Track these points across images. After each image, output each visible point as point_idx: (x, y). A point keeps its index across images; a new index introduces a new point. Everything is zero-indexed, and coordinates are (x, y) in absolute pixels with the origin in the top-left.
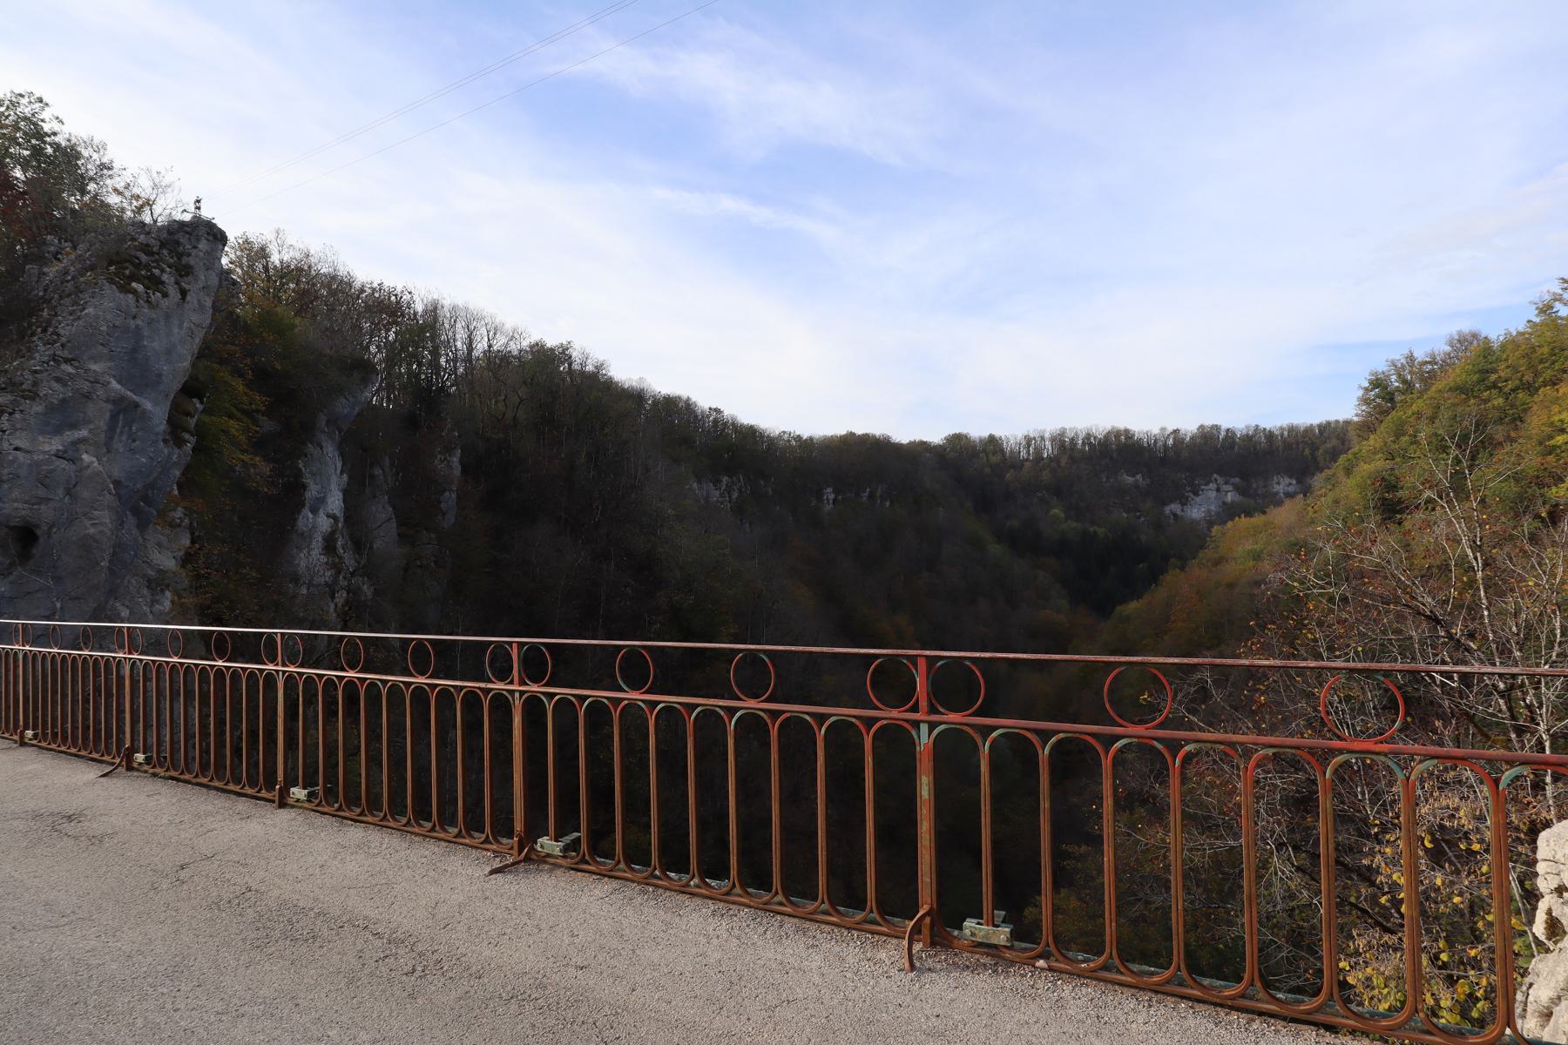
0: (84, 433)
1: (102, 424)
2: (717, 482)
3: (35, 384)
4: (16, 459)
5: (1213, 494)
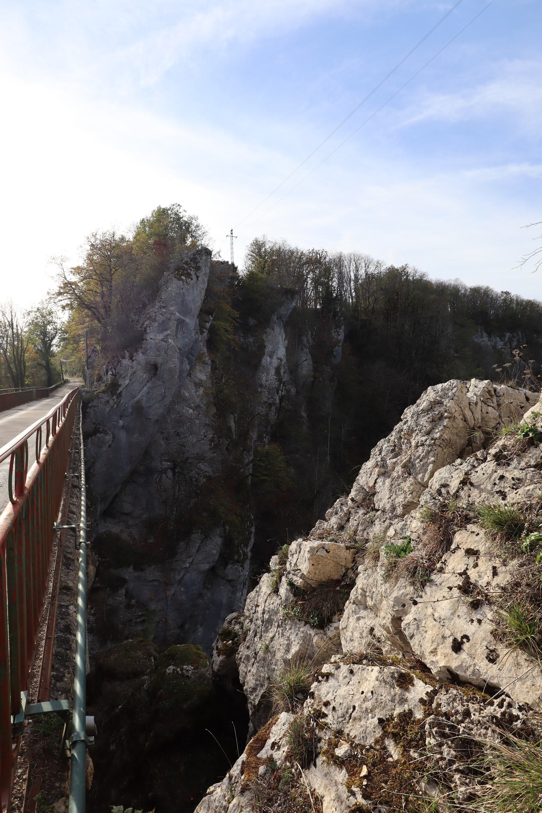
0: (169, 332)
1: (174, 328)
2: (502, 337)
3: (156, 316)
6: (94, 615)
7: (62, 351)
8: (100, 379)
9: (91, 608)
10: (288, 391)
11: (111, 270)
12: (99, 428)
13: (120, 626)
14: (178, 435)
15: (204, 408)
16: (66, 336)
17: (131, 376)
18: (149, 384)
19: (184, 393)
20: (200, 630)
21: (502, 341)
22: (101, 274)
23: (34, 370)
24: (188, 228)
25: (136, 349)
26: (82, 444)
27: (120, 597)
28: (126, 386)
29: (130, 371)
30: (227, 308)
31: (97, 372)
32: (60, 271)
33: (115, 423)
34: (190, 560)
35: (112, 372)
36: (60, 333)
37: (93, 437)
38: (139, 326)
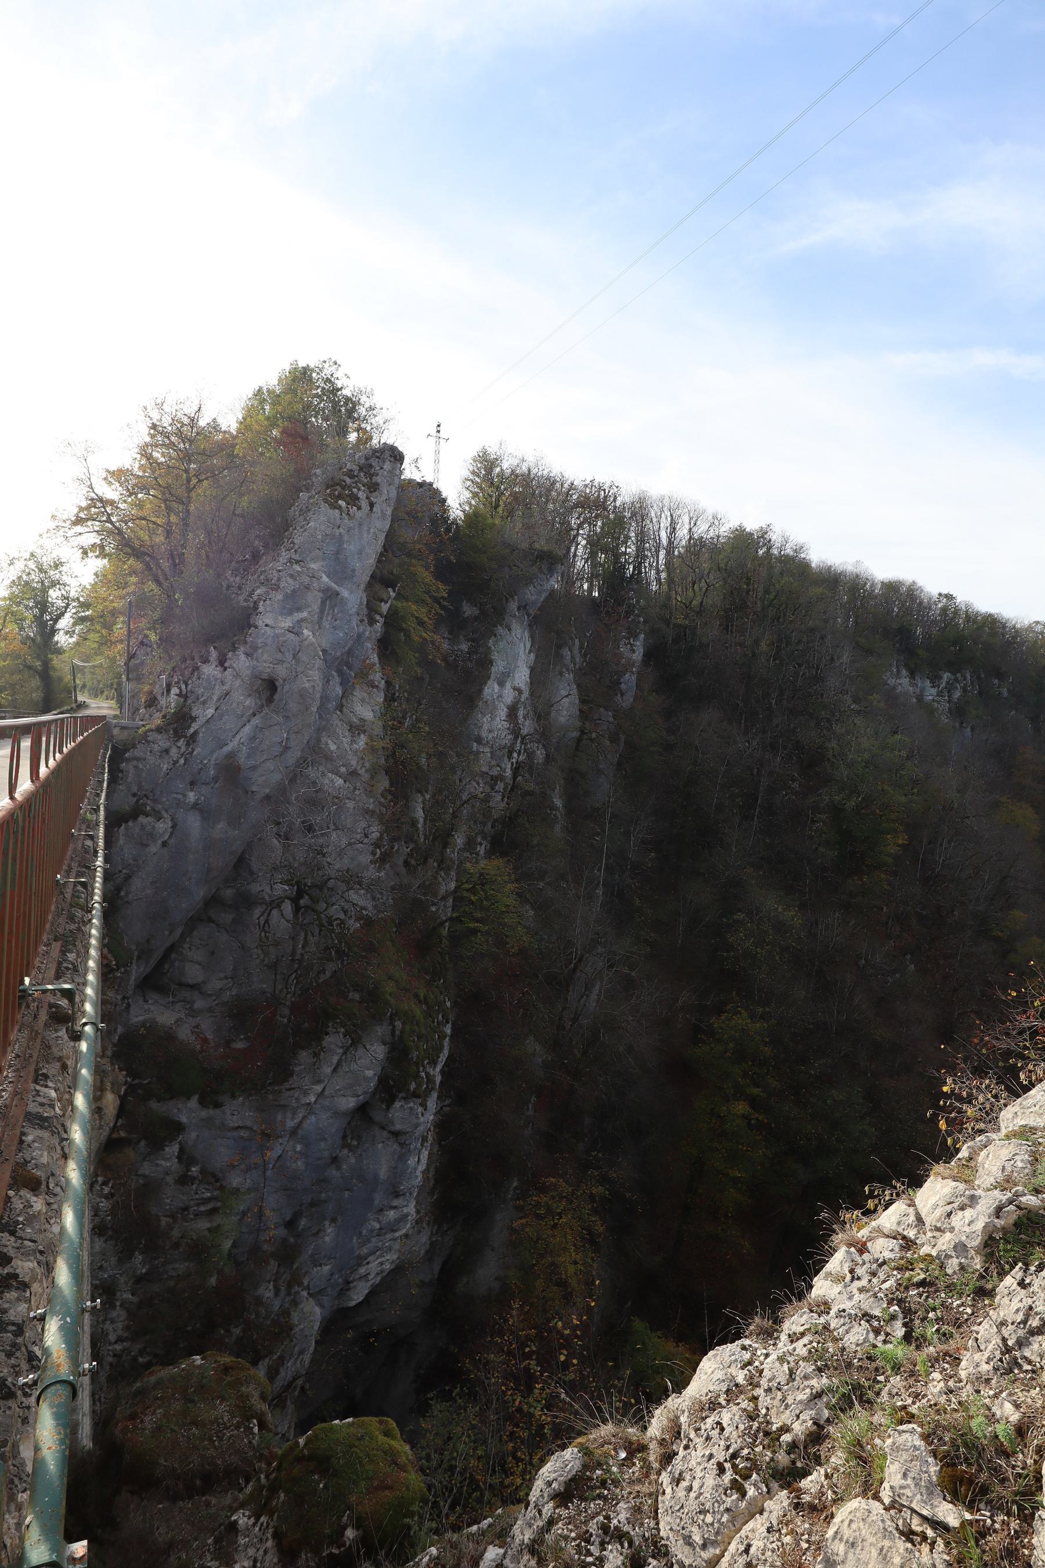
0: (305, 614)
1: (316, 607)
2: (935, 679)
3: (279, 580)
6: (109, 1196)
7: (77, 644)
8: (152, 702)
9: (105, 1183)
10: (530, 755)
11: (189, 480)
12: (145, 805)
13: (164, 1221)
14: (310, 829)
15: (366, 777)
16: (87, 613)
17: (219, 700)
18: (256, 721)
19: (327, 744)
20: (329, 1231)
21: (934, 687)
22: (168, 487)
23: (16, 677)
24: (350, 412)
25: (233, 644)
26: (101, 853)
27: (166, 1160)
28: (207, 721)
29: (218, 691)
30: (426, 576)
31: (147, 688)
32: (81, 472)
33: (180, 796)
34: (318, 1088)
35: (180, 688)
36: (74, 607)
37: (130, 824)
38: (241, 598)
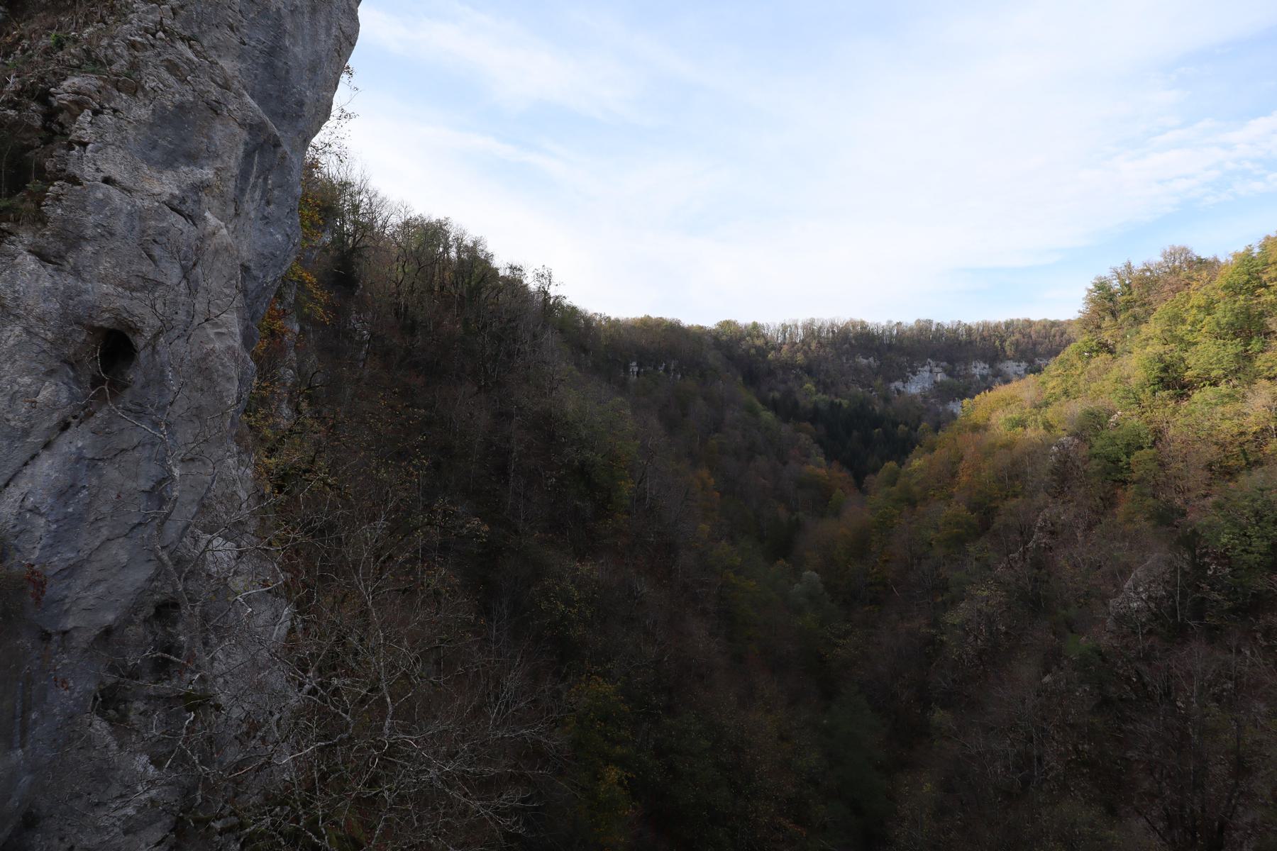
0: (207, 173)
1: (233, 162)
3: (134, 66)
4: (106, 201)
5: (927, 375)
